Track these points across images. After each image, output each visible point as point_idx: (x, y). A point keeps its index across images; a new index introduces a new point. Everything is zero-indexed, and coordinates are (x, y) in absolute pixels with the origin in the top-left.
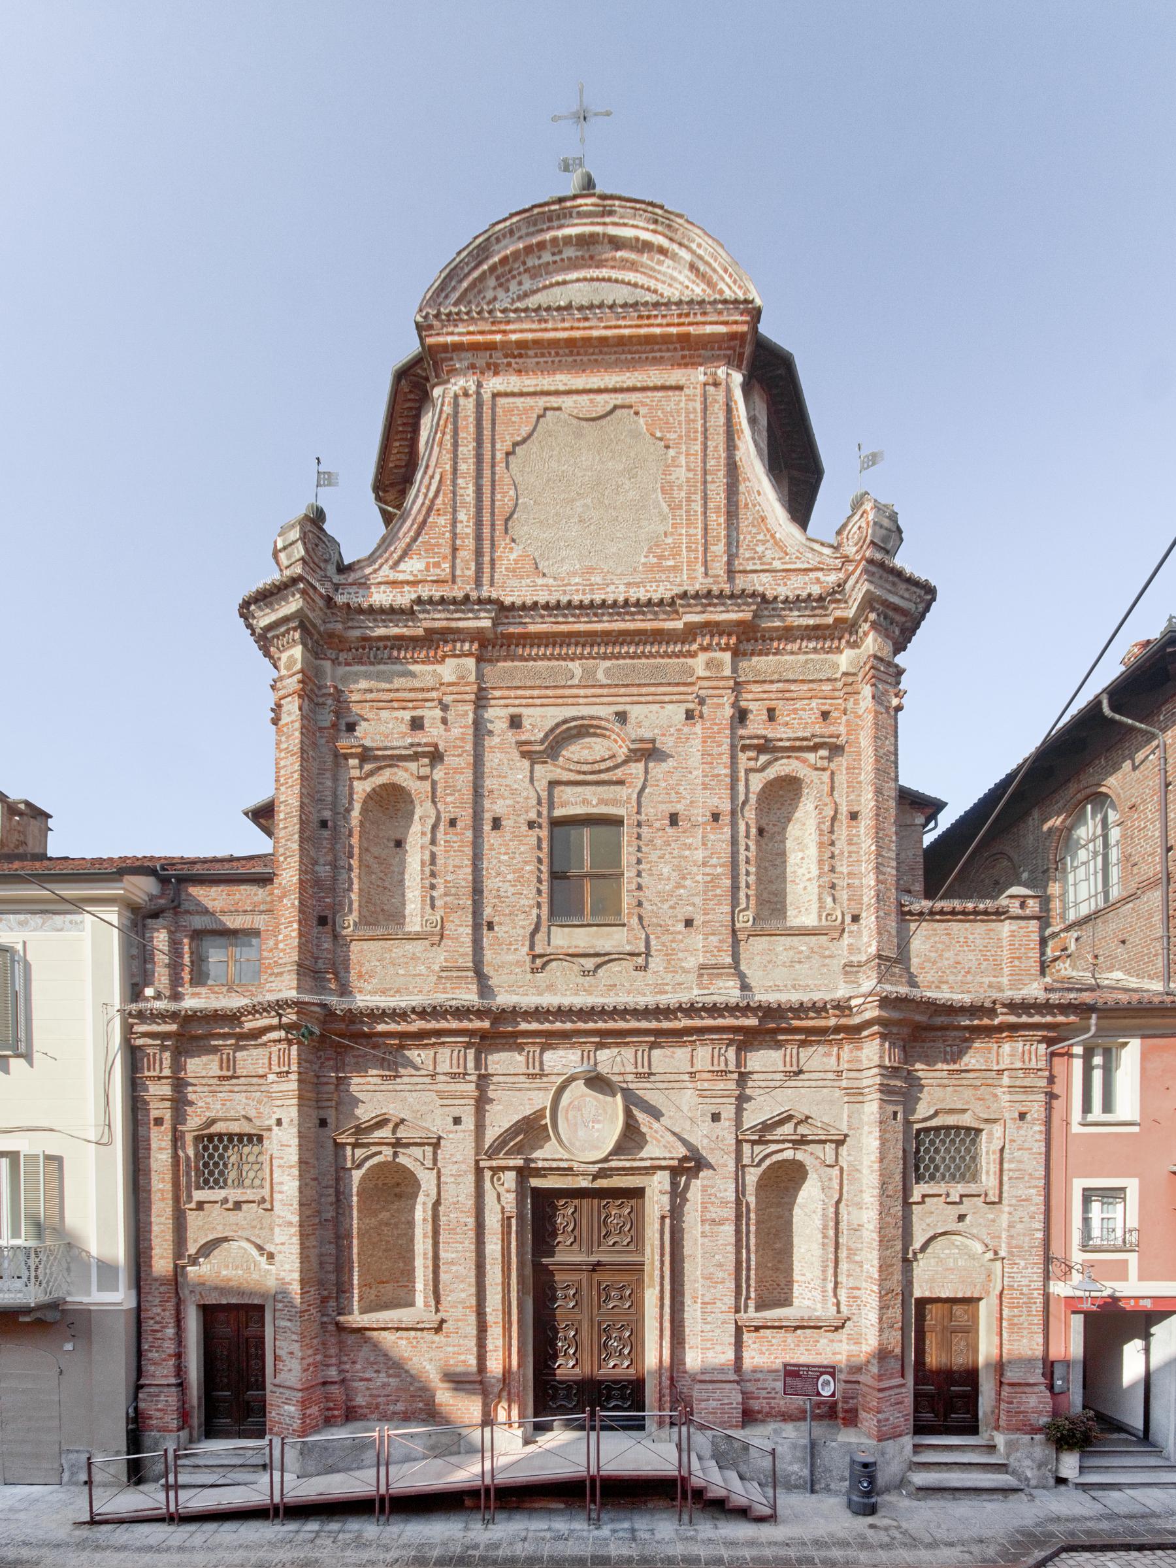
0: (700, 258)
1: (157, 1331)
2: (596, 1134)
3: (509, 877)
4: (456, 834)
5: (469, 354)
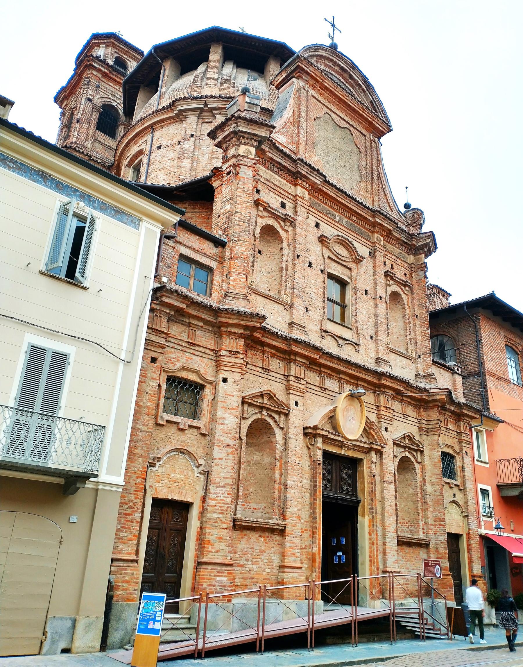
0: (374, 101)
1: (129, 515)
3: (314, 291)
5: (309, 78)
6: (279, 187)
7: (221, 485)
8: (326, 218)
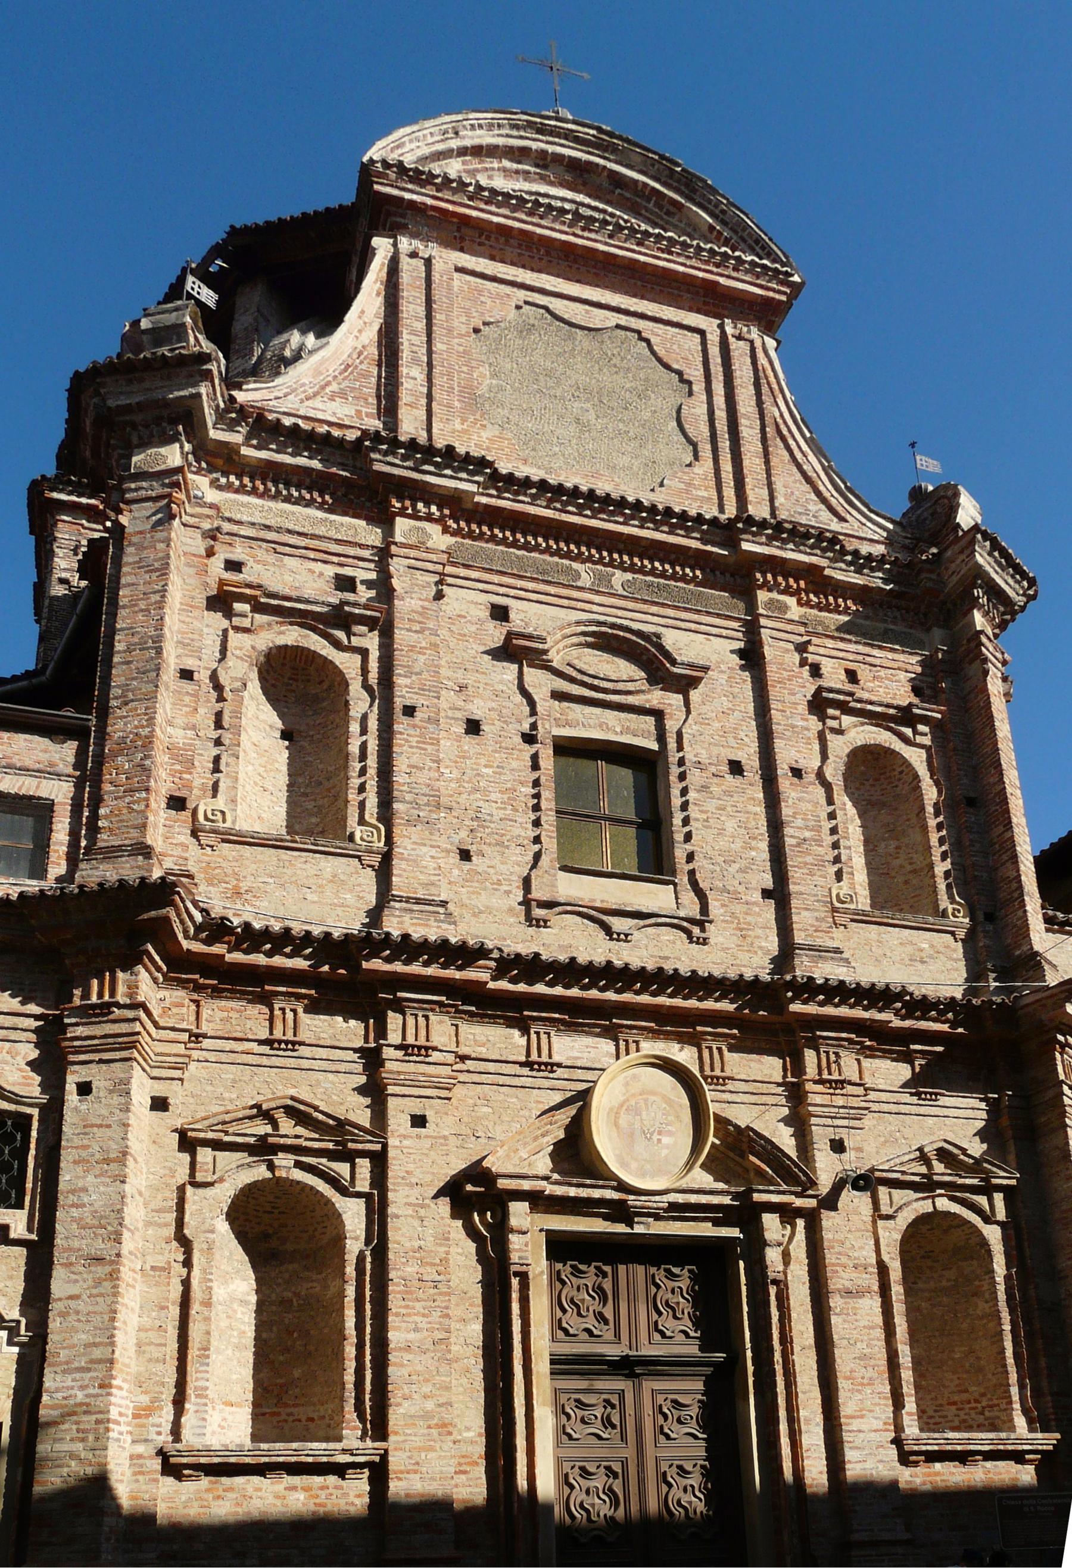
2: (664, 1152)
4: (414, 726)
6: (314, 537)
7: (76, 1364)
8: (531, 585)
